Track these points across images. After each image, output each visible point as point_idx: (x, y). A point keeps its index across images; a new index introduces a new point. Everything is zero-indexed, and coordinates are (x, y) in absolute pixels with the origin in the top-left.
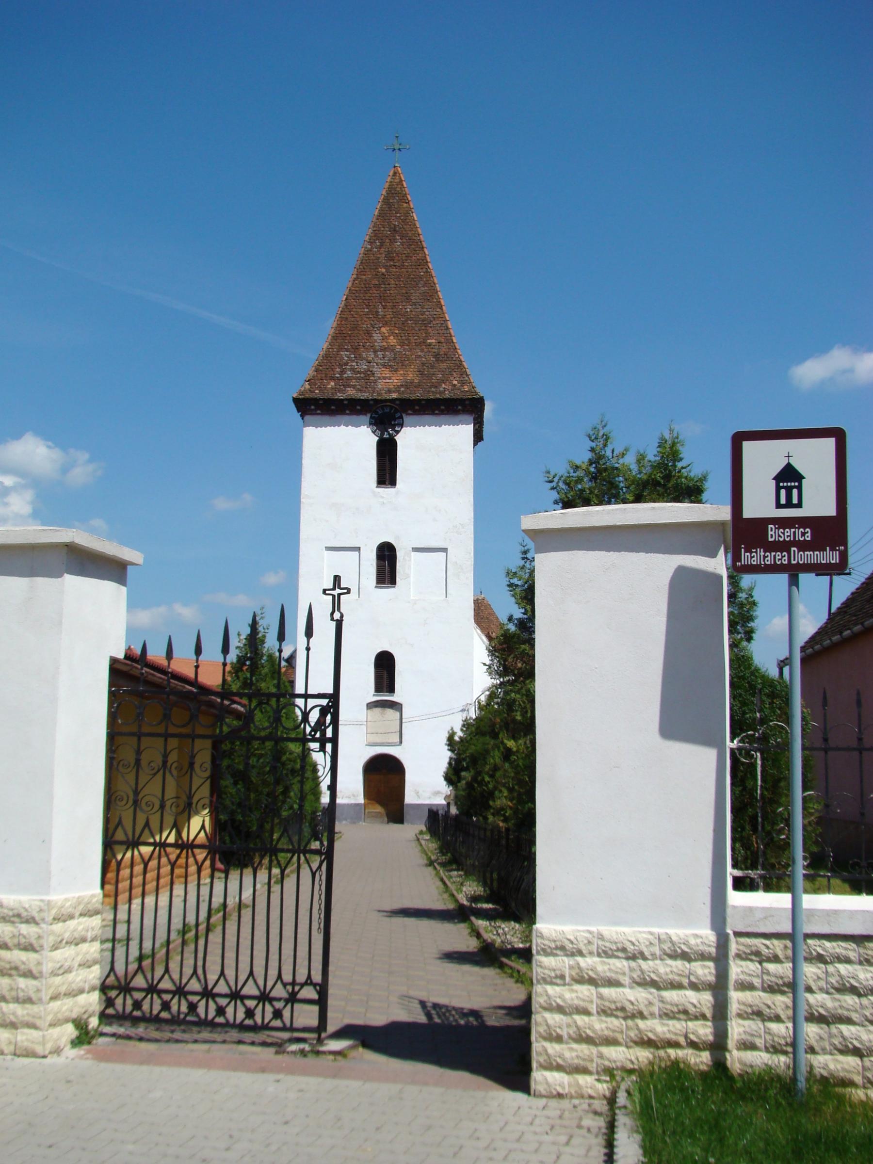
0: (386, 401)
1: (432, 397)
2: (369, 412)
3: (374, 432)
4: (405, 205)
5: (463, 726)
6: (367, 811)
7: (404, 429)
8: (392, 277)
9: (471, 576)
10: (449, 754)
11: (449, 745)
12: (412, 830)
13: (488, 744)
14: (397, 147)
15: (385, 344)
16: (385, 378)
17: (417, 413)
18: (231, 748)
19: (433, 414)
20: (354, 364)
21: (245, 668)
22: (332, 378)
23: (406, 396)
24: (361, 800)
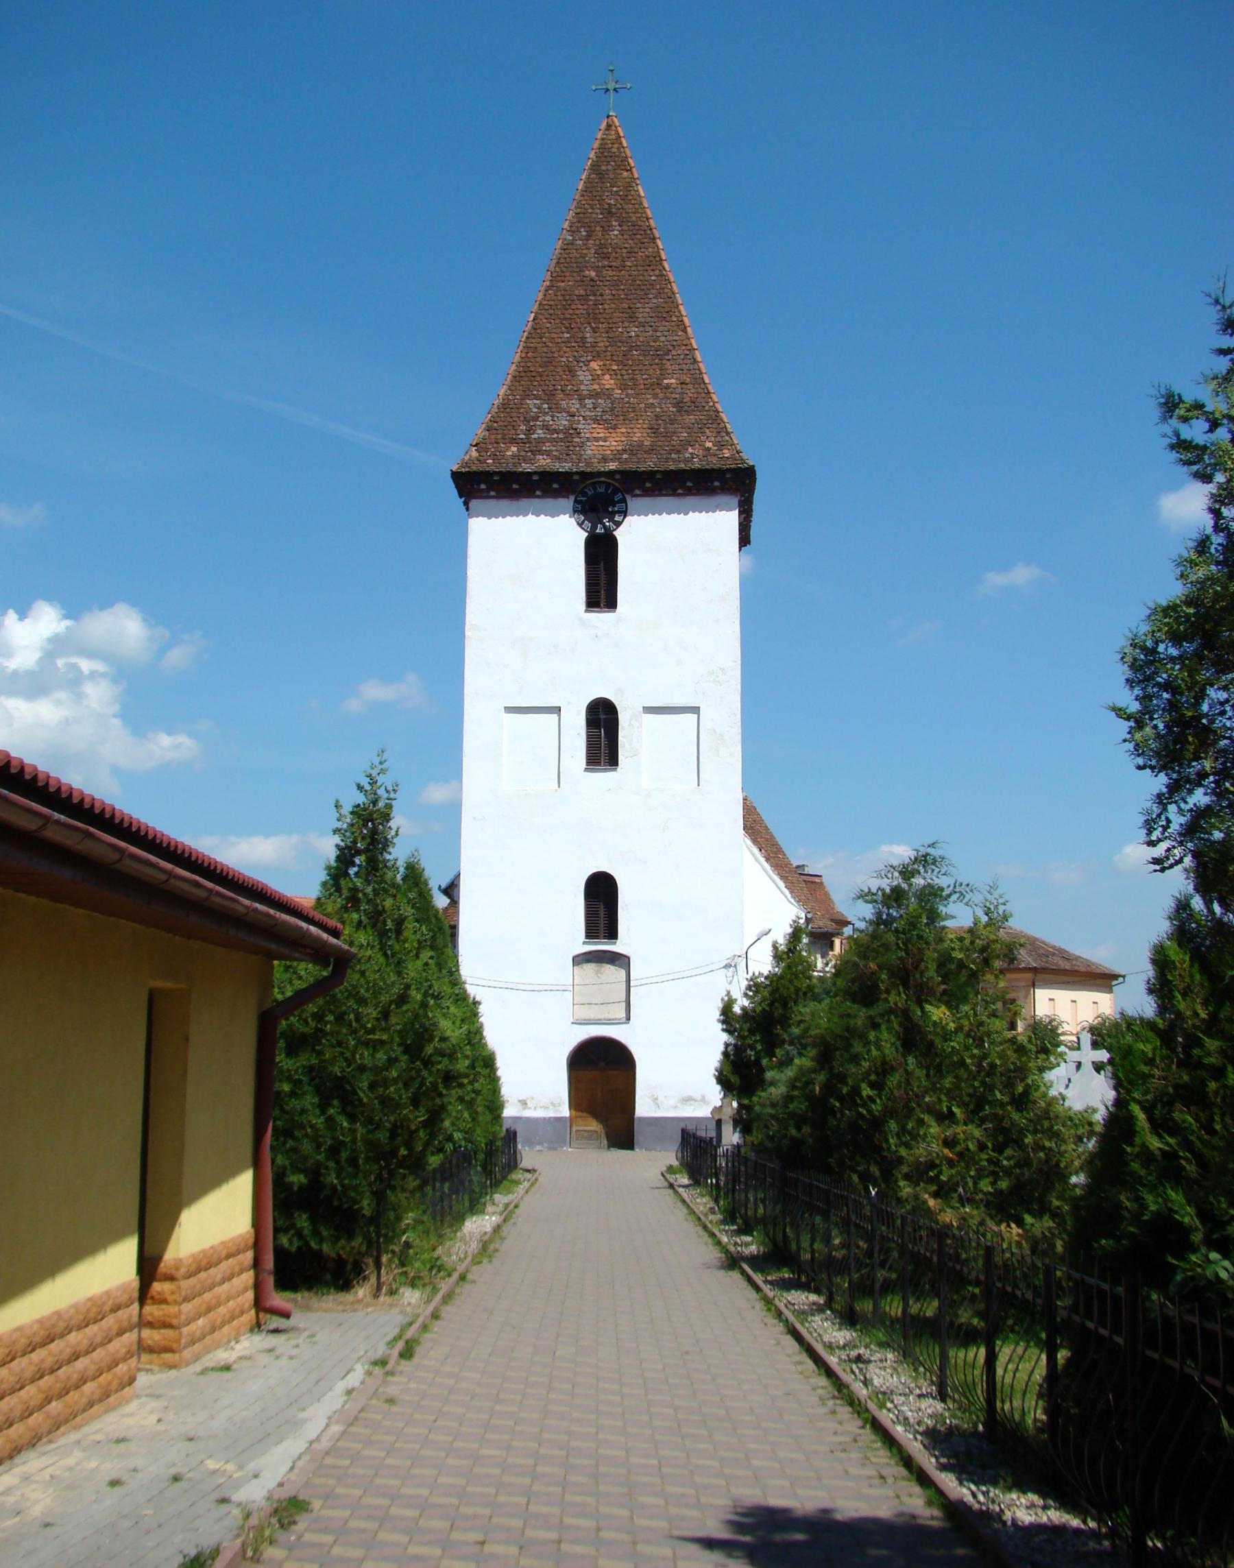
0: (600, 474)
1: (672, 467)
3: (580, 525)
4: (625, 174)
5: (749, 988)
6: (574, 1129)
7: (628, 519)
8: (607, 281)
9: (738, 749)
10: (725, 1037)
11: (723, 1022)
12: (652, 1163)
13: (855, 1017)
14: (611, 86)
15: (596, 387)
16: (597, 439)
17: (648, 493)
18: (317, 1030)
19: (674, 494)
20: (548, 418)
21: (352, 871)
22: (514, 441)
23: (632, 466)
24: (565, 1112)
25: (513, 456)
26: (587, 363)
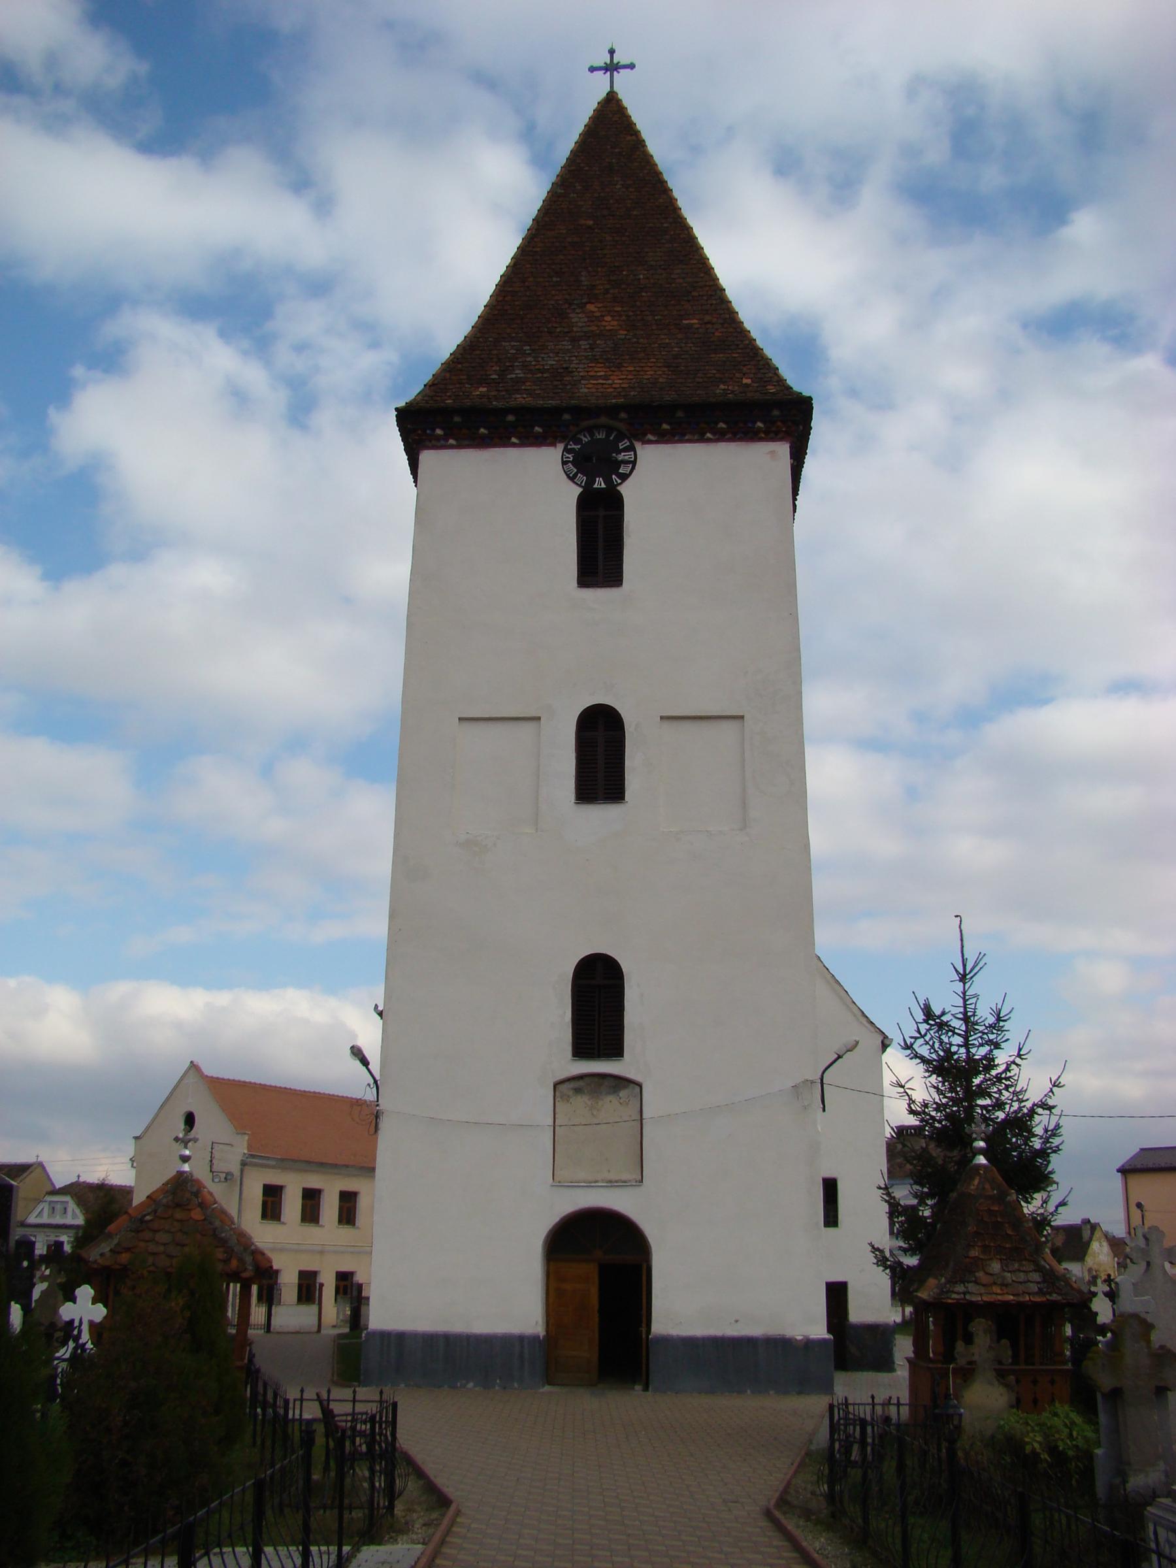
2: (563, 438)
19: (702, 439)
25: (482, 396)
26: (582, 306)
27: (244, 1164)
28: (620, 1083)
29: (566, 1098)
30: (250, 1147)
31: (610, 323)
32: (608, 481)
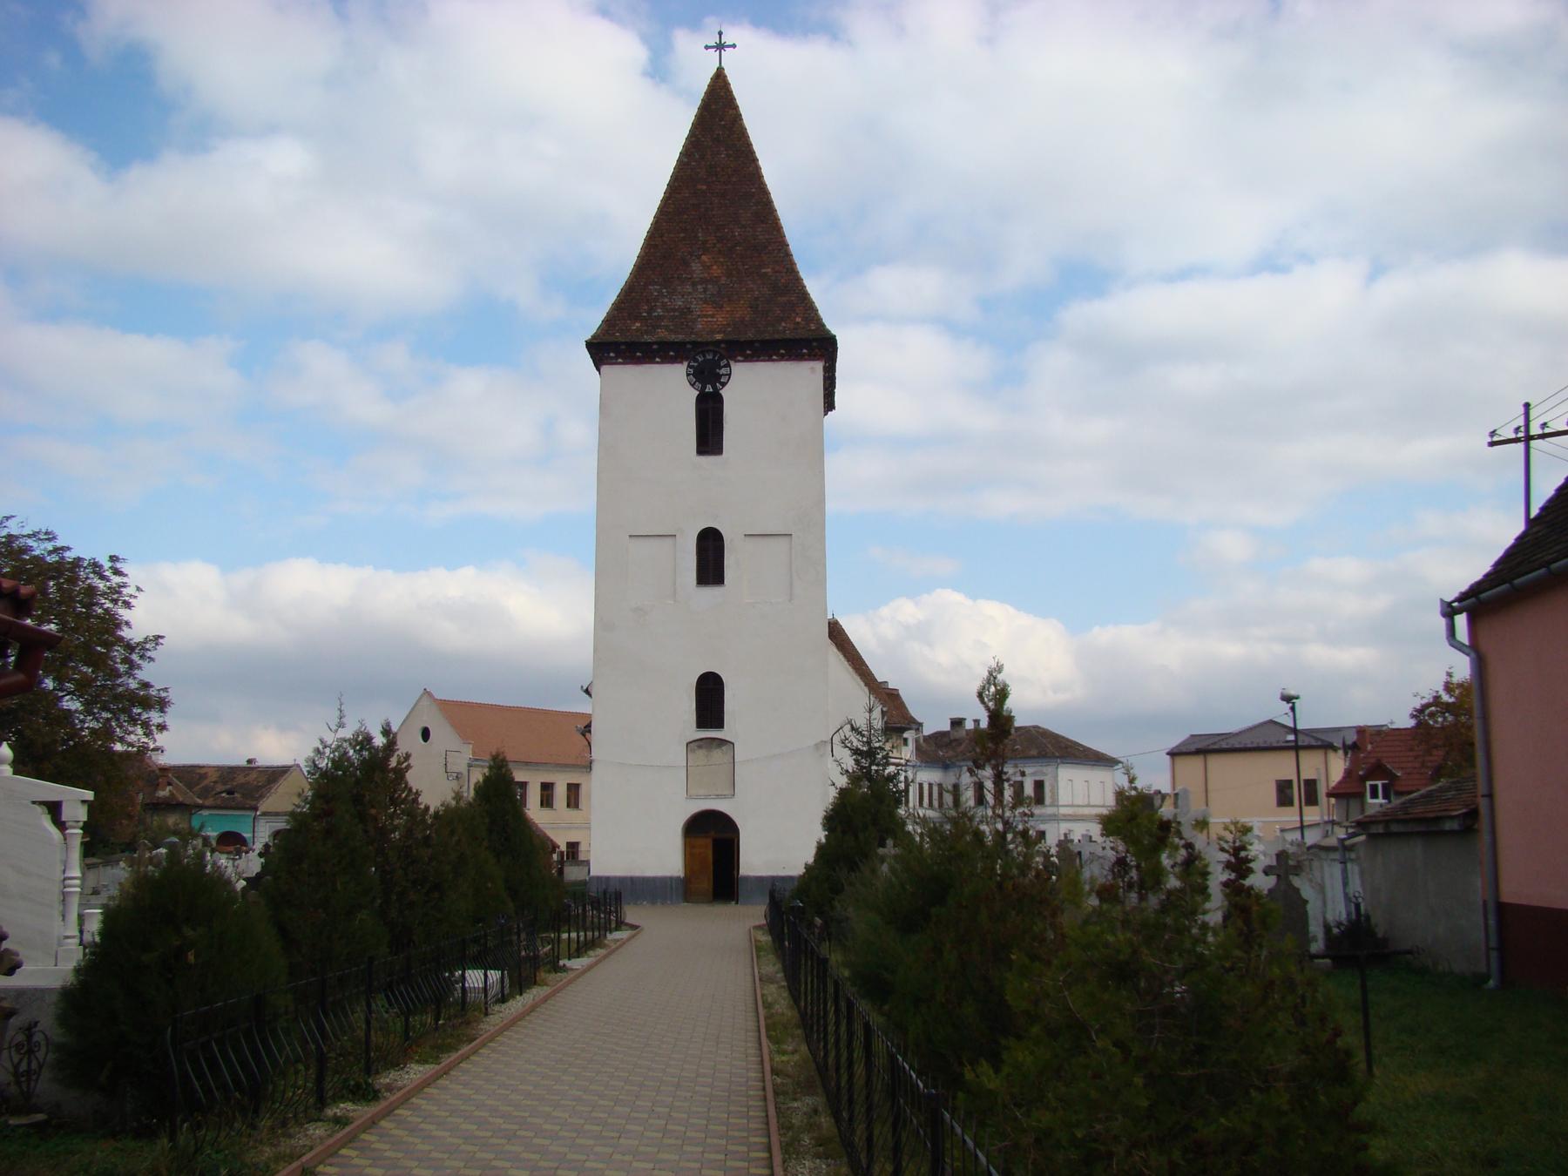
0: (707, 344)
17: (748, 359)
22: (637, 318)
25: (637, 330)
26: (699, 257)
27: (470, 766)
28: (722, 742)
29: (693, 751)
30: (474, 753)
31: (716, 271)
32: (714, 387)
